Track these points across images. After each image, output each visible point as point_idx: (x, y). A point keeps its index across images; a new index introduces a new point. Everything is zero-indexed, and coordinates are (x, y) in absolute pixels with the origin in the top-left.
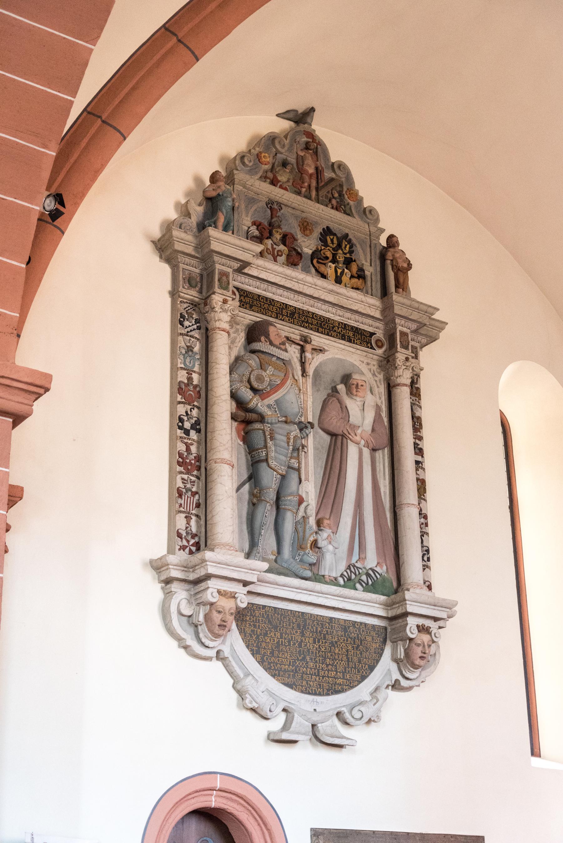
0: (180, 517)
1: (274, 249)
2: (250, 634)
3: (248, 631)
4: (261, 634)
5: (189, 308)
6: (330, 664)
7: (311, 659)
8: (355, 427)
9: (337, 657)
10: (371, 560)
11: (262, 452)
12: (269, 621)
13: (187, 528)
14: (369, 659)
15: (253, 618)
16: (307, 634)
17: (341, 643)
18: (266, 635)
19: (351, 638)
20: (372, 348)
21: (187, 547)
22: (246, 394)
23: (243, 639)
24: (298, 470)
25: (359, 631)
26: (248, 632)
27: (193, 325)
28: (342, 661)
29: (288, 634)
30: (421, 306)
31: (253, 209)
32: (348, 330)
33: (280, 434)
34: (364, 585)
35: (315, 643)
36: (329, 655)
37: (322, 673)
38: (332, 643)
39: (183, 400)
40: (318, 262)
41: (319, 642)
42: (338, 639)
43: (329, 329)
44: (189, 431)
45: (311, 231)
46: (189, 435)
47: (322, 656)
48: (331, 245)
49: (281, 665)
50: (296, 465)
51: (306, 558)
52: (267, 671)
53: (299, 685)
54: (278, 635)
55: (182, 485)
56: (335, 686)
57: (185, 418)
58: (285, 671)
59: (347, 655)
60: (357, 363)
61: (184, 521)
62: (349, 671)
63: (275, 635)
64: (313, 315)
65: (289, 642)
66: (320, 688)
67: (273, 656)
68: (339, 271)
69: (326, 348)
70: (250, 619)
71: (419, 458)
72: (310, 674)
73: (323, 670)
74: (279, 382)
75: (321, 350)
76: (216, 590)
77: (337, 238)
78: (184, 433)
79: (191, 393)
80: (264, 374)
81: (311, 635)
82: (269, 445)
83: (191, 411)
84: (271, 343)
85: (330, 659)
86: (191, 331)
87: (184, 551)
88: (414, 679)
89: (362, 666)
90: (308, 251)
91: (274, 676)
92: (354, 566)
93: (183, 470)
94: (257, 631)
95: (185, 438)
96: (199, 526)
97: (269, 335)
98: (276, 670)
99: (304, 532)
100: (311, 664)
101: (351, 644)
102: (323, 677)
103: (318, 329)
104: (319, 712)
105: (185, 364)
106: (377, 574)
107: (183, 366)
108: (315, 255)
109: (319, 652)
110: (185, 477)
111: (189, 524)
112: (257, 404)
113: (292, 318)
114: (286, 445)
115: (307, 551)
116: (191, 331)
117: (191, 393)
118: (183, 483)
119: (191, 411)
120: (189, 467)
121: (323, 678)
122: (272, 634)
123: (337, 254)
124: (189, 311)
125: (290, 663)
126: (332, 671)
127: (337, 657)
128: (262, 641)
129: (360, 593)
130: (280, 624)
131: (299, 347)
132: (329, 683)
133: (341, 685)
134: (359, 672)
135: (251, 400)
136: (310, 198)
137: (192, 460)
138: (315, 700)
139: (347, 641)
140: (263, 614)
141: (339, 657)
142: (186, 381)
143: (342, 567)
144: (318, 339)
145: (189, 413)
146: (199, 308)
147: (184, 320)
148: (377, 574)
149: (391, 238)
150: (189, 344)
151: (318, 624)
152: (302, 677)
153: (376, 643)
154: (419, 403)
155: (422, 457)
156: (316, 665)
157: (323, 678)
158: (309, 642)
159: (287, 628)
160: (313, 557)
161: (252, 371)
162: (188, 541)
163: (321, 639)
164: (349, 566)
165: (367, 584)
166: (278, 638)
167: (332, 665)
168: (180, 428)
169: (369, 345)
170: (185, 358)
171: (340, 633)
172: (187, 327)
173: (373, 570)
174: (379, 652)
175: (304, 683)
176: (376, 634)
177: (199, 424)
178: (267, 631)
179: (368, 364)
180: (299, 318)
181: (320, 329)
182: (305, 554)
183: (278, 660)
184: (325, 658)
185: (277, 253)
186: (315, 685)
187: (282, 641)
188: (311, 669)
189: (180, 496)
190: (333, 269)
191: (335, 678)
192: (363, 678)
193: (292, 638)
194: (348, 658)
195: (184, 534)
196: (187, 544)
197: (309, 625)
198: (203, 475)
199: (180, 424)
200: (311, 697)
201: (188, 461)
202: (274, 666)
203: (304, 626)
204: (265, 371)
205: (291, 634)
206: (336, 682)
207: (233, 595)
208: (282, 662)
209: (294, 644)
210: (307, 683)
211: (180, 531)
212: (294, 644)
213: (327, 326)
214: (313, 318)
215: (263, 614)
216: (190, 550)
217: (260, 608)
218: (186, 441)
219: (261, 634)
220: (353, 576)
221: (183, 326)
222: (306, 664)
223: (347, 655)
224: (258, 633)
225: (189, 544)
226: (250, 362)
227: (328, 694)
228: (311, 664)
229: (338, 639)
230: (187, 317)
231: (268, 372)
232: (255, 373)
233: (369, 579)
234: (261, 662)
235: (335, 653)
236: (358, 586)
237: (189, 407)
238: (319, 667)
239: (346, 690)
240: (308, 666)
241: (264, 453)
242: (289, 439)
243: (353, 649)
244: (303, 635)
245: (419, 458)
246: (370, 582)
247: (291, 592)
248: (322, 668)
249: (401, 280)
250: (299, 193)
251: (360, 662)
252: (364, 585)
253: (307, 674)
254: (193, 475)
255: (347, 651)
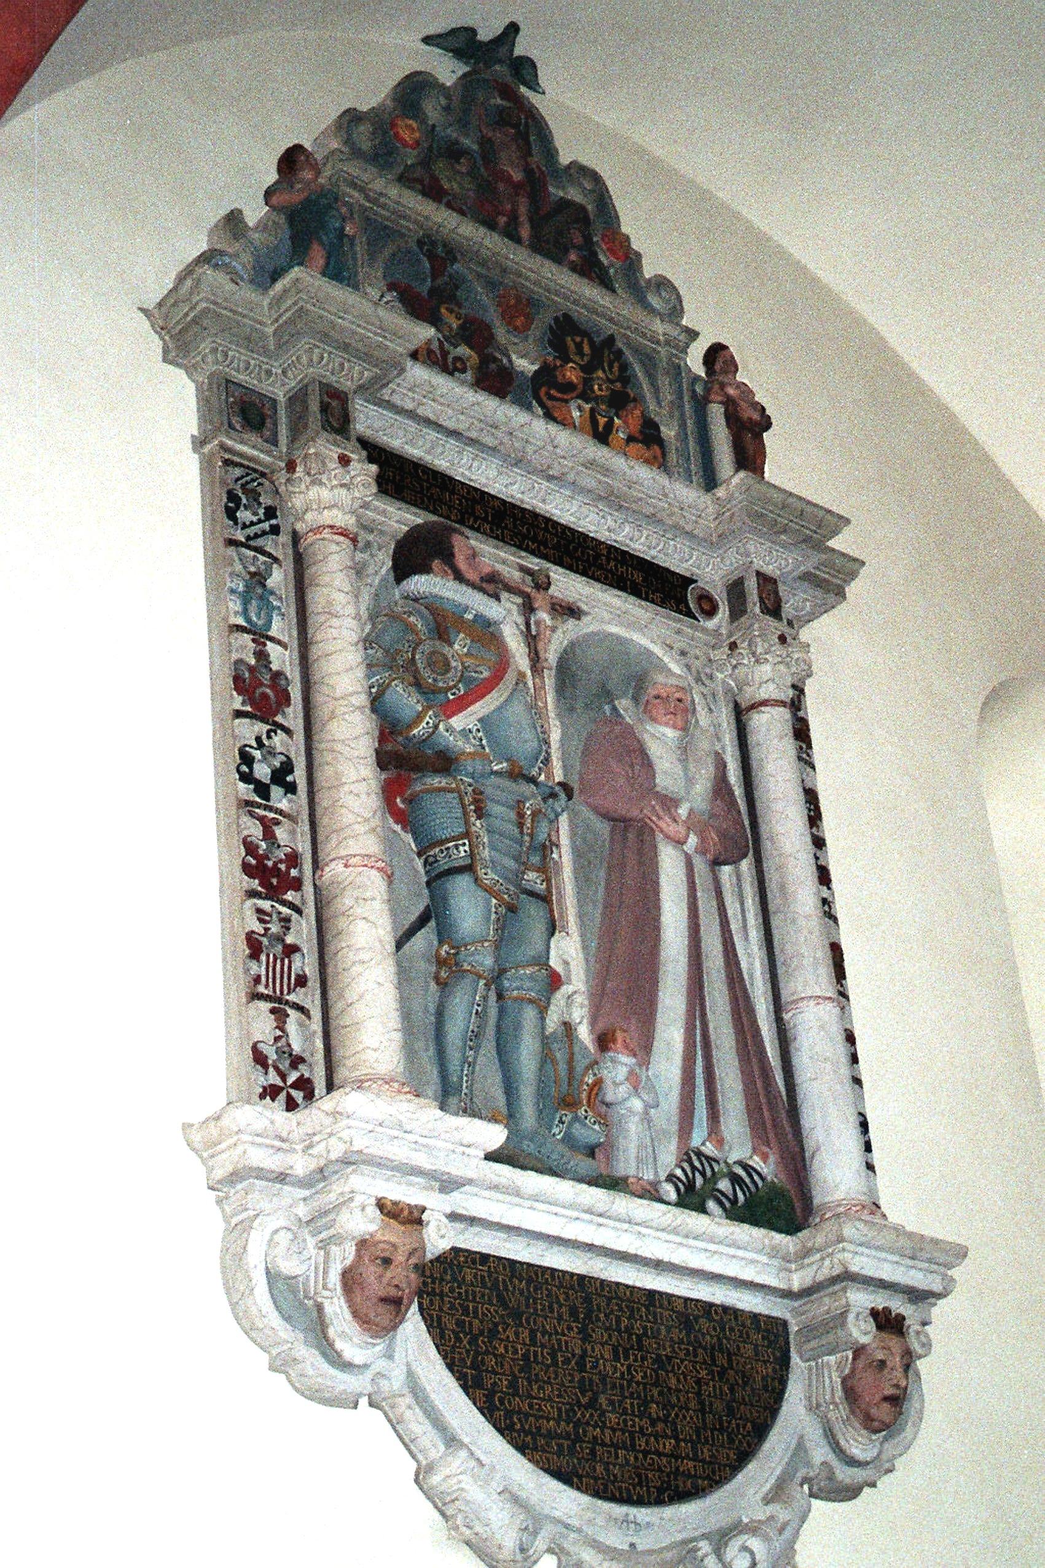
0: (257, 1009)
1: (445, 354)
2: (453, 1331)
3: (450, 1324)
4: (482, 1333)
5: (248, 478)
6: (659, 1418)
7: (611, 1403)
8: (669, 803)
9: (674, 1400)
10: (737, 1145)
11: (457, 847)
12: (499, 1296)
13: (277, 1039)
14: (752, 1405)
15: (459, 1287)
16: (598, 1334)
17: (682, 1361)
18: (493, 1333)
19: (705, 1349)
20: (689, 614)
21: (282, 1089)
22: (405, 700)
23: (437, 1347)
24: (545, 899)
25: (723, 1329)
26: (449, 1326)
27: (260, 521)
28: (688, 1410)
29: (550, 1335)
30: (809, 509)
31: (387, 253)
32: (631, 566)
33: (498, 802)
34: (728, 1205)
35: (617, 1358)
36: (655, 1392)
37: (641, 1443)
38: (658, 1360)
39: (248, 708)
40: (548, 394)
41: (627, 1358)
42: (674, 1351)
43: (588, 561)
44: (267, 787)
45: (529, 319)
46: (268, 799)
47: (639, 1397)
48: (577, 358)
49: (538, 1418)
50: (541, 887)
51: (578, 1130)
52: (502, 1434)
53: (588, 1475)
54: (525, 1335)
55: (258, 928)
56: (676, 1479)
57: (257, 754)
58: (550, 1435)
59: (698, 1394)
60: (657, 650)
61: (270, 1021)
62: (706, 1439)
63: (517, 1334)
64: (546, 524)
65: (553, 1355)
66: (640, 1484)
67: (516, 1394)
68: (602, 421)
69: (584, 607)
70: (452, 1290)
71: (825, 893)
72: (612, 1445)
73: (644, 1435)
74: (486, 674)
75: (572, 611)
76: (373, 1201)
77: (592, 343)
78: (255, 791)
79: (268, 691)
80: (446, 650)
81: (606, 1336)
82: (474, 829)
83: (269, 737)
84: (459, 577)
85: (657, 1404)
86: (256, 536)
87: (273, 1100)
88: (867, 1463)
89: (738, 1425)
90: (525, 366)
91: (521, 1448)
92: (699, 1154)
93: (260, 889)
94: (470, 1324)
95: (259, 806)
96: (308, 1038)
97: (452, 555)
98: (526, 1434)
99: (571, 1061)
100: (612, 1418)
101: (705, 1362)
102: (646, 1453)
103: (561, 558)
104: (644, 1552)
105: (245, 613)
106: (756, 1177)
107: (241, 621)
108: (545, 377)
109: (629, 1382)
110: (266, 905)
111: (282, 1030)
112: (436, 727)
113: (499, 526)
114: (517, 831)
115: (581, 1112)
116: (256, 536)
117: (268, 691)
118: (261, 921)
119: (269, 737)
120: (274, 881)
121: (645, 1458)
122: (510, 1333)
123: (592, 379)
124: (249, 486)
125: (560, 1415)
126: (666, 1437)
127: (674, 1400)
128: (487, 1352)
129: (712, 1224)
130: (528, 1306)
131: (519, 600)
132: (660, 1470)
133: (689, 1476)
134: (731, 1441)
135: (419, 717)
136: (518, 241)
137: (281, 861)
138: (631, 1518)
139: (695, 1356)
140: (483, 1277)
141: (679, 1400)
142: (253, 662)
143: (668, 1157)
144: (567, 584)
145: (266, 742)
146: (272, 482)
147: (238, 508)
148: (756, 1177)
149: (716, 354)
150: (253, 569)
151: (621, 1309)
152: (593, 1452)
153: (765, 1362)
154: (808, 755)
155: (829, 888)
156: (625, 1421)
157: (645, 1458)
158: (602, 1357)
159: (546, 1317)
160: (596, 1127)
161: (418, 645)
162: (283, 1076)
163: (632, 1348)
164: (687, 1154)
165: (734, 1201)
166: (524, 1344)
167: (665, 1421)
168: (246, 778)
169: (682, 607)
170: (246, 603)
171: (675, 1334)
172: (245, 526)
173: (746, 1167)
174: (773, 1390)
175: (599, 1468)
176: (763, 1338)
177: (291, 771)
178: (496, 1325)
179: (683, 653)
180: (515, 526)
181: (567, 559)
182: (576, 1118)
183: (531, 1406)
184: (645, 1403)
185: (454, 363)
186: (626, 1476)
187: (535, 1353)
188: (614, 1430)
189: (255, 955)
190: (587, 414)
191: (676, 1458)
192: (744, 1456)
193: (559, 1345)
194: (702, 1403)
195: (272, 1056)
196: (282, 1084)
197: (599, 1310)
198: (311, 904)
199: (244, 768)
200: (619, 1510)
201: (270, 863)
202: (519, 1420)
203: (588, 1316)
204: (451, 645)
205: (557, 1333)
206: (677, 1469)
207: (416, 1214)
208: (540, 1409)
209: (567, 1361)
210: (607, 1470)
211: (260, 1046)
212: (567, 1361)
213: (582, 553)
214: (546, 529)
215: (483, 1277)
216: (289, 1098)
217: (474, 1262)
218: (260, 812)
219: (482, 1333)
220: (699, 1181)
221: (236, 523)
222: (600, 1416)
223: (698, 1394)
224: (475, 1331)
225: (284, 1081)
226: (412, 619)
227: (659, 1502)
228: (612, 1418)
229: (674, 1351)
230: (244, 501)
231: (456, 647)
232: (426, 647)
233: (738, 1188)
234: (488, 1410)
235: (670, 1389)
236: (711, 1205)
237: (262, 728)
238: (633, 1426)
239: (703, 1490)
240: (604, 1423)
241: (461, 848)
242: (521, 815)
243: (713, 1379)
244: (586, 1337)
245: (825, 893)
246: (741, 1197)
247: (551, 1222)
248: (641, 1428)
249: (751, 449)
250: (491, 226)
251: (731, 1412)
252: (728, 1205)
253: (603, 1444)
254: (284, 903)
255: (698, 1382)
